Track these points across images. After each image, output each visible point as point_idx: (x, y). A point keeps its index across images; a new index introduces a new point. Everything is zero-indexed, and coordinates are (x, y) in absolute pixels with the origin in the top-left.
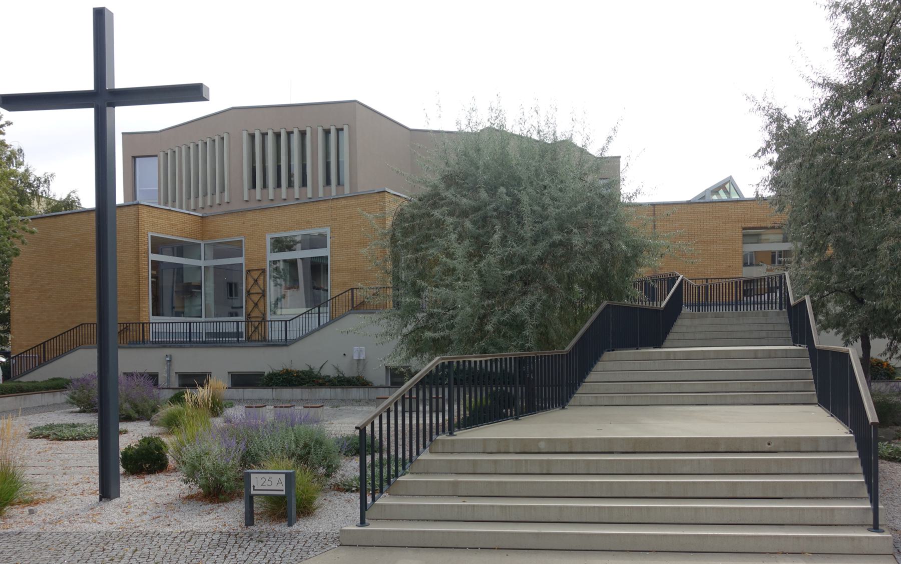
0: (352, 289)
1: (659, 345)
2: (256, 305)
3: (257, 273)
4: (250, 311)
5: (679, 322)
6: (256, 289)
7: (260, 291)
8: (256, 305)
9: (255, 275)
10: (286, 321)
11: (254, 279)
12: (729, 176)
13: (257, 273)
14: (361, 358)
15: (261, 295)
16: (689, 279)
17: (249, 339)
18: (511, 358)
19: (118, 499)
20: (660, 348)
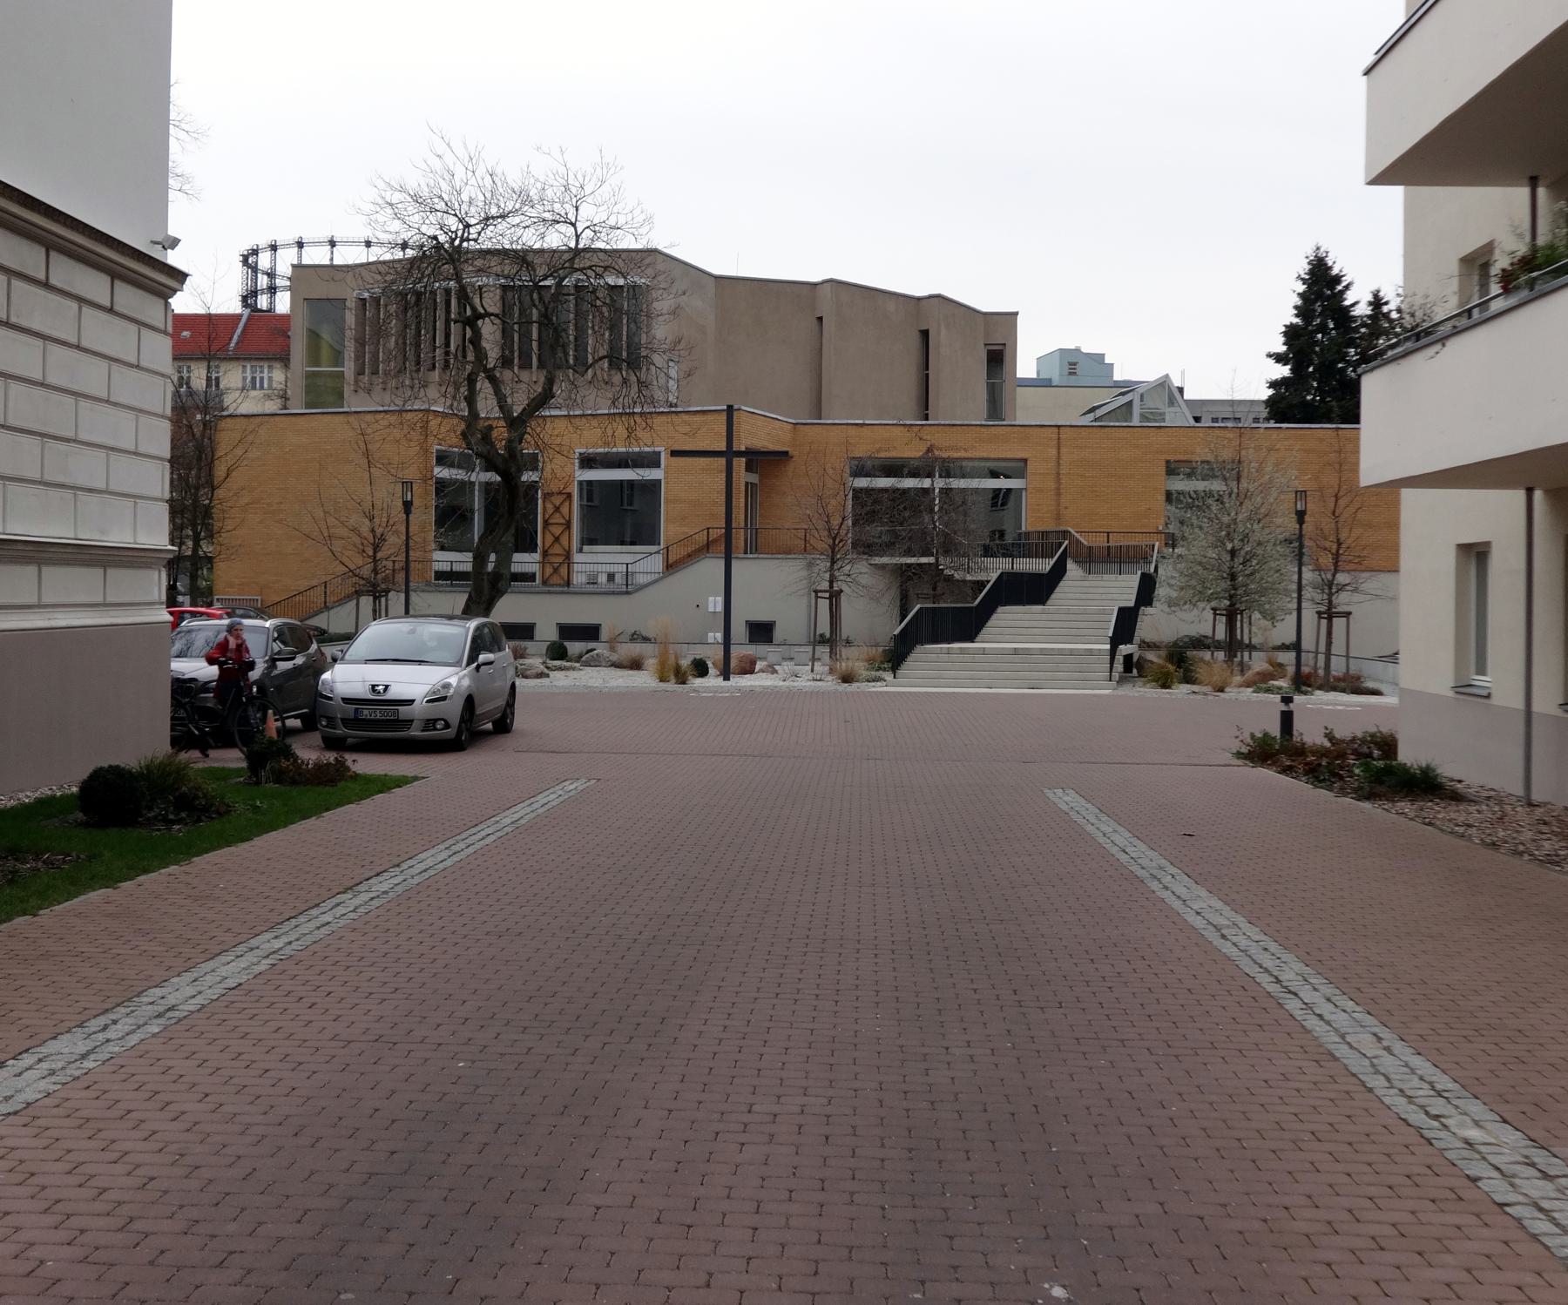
0: (708, 529)
1: (972, 640)
2: (557, 539)
3: (561, 498)
4: (554, 552)
5: (1061, 584)
6: (557, 519)
7: (563, 521)
8: (557, 539)
9: (557, 500)
10: (627, 564)
11: (555, 506)
12: (1165, 373)
13: (561, 498)
14: (717, 610)
15: (565, 526)
16: (1077, 532)
17: (545, 582)
18: (657, 465)
19: (1121, 606)
20: (973, 642)
